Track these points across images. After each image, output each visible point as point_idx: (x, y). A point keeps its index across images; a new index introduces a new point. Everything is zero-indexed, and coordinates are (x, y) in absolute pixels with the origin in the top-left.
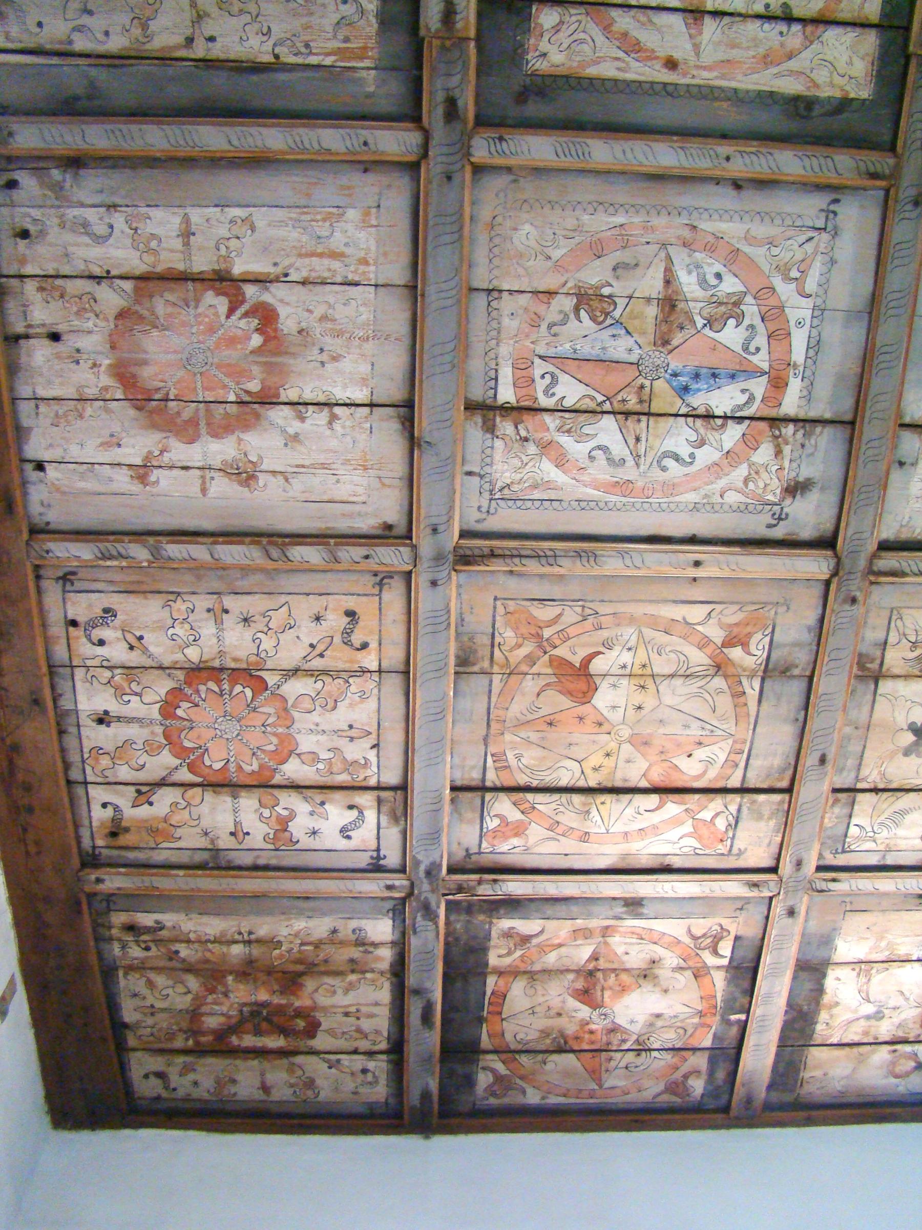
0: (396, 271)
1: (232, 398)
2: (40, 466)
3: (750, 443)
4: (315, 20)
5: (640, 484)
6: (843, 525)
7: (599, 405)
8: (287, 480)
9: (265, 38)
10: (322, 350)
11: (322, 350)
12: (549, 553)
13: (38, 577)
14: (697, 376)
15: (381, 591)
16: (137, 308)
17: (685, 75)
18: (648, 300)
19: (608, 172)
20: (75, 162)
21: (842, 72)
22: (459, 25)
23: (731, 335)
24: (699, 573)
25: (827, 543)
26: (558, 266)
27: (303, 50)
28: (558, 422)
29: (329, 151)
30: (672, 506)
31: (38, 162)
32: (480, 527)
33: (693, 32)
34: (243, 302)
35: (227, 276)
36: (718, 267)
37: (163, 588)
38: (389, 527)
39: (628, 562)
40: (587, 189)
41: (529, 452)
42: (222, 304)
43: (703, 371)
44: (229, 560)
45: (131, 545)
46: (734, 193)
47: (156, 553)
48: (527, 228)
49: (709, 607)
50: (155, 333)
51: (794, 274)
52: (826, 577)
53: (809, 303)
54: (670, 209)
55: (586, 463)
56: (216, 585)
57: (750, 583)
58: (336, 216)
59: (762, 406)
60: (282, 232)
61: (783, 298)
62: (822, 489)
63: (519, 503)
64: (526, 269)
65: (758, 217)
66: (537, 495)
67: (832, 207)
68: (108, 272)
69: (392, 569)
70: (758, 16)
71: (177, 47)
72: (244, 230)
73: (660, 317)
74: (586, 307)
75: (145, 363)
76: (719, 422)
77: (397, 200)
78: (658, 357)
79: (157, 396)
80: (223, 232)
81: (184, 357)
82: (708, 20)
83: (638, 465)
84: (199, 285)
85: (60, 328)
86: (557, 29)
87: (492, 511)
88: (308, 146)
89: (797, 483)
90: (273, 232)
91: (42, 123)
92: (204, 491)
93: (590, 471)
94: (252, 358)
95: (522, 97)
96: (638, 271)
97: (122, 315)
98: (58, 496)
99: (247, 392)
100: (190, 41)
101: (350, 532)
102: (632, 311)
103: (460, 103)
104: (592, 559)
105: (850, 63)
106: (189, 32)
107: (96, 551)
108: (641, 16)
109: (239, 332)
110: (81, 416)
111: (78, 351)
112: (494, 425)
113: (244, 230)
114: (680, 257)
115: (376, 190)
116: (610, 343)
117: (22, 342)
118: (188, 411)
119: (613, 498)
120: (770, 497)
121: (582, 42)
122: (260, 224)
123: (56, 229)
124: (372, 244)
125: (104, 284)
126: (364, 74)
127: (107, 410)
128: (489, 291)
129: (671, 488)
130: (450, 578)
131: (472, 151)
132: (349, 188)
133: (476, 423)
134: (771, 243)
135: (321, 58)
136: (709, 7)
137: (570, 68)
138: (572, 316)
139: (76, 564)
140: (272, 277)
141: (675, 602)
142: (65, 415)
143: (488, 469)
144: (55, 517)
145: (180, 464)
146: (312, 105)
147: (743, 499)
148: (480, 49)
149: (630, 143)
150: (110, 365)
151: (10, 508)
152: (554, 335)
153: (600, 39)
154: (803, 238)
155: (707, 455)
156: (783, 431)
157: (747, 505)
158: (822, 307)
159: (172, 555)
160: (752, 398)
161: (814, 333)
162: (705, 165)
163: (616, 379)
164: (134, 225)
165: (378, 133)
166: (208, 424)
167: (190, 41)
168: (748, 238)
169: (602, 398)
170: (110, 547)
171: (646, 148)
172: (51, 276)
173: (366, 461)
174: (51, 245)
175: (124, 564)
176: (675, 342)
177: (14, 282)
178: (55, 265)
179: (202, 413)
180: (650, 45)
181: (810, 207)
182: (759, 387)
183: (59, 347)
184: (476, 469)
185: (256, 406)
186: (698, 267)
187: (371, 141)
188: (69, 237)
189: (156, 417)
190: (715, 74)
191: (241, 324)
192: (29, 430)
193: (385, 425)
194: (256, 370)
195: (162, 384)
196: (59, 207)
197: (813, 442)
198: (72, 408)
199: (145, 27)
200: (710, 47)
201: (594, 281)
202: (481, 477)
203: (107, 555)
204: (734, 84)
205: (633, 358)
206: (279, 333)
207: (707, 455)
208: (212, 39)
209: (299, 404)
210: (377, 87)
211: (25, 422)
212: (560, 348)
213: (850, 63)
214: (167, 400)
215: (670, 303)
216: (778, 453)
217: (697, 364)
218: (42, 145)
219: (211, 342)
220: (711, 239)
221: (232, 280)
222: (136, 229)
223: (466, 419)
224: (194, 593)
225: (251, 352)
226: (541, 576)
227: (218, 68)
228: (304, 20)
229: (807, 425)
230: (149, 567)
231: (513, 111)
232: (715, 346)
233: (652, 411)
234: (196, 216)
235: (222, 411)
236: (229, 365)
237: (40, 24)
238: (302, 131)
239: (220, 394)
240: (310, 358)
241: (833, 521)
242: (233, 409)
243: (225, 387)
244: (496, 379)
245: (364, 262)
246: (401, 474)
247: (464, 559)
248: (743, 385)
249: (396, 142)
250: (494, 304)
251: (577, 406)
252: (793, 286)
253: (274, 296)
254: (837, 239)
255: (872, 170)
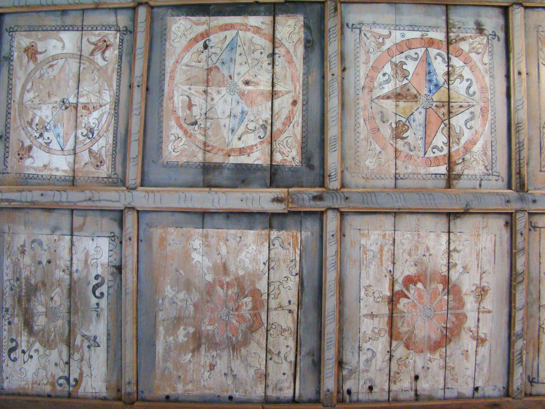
0: (388, 221)
1: (446, 297)
2: (476, 389)
3: (459, 53)
4: (282, 258)
5: (482, 104)
6: (496, 4)
7: (446, 126)
8: (484, 272)
9: (289, 279)
10: (424, 255)
11: (424, 255)
12: (517, 146)
13: (531, 395)
14: (430, 81)
15: (538, 227)
16: (404, 339)
17: (299, 97)
18: (397, 106)
19: (342, 127)
20: (340, 364)
21: (293, 29)
22: (283, 196)
23: (410, 67)
24: (524, 72)
25: (505, 11)
26: (384, 148)
27: (294, 263)
28: (454, 145)
29: (336, 252)
30: (492, 88)
31: (340, 380)
32: (506, 179)
33: (281, 95)
34: (402, 291)
35: (391, 298)
36: (380, 75)
37: (537, 333)
38: (507, 224)
39: (520, 107)
40: (349, 136)
41: (469, 157)
42: (403, 301)
43: (428, 78)
44: (523, 301)
45: (515, 348)
46: (347, 70)
47: (520, 336)
48: (367, 163)
49: (541, 65)
50: (416, 332)
51: (381, 40)
52: (522, 8)
53: (393, 32)
54: (356, 99)
55: (473, 131)
56: (535, 307)
57: (527, 46)
58: (365, 250)
59: (442, 49)
60: (372, 273)
61: (392, 44)
62: (479, 16)
63: (494, 161)
64: (386, 163)
65: (357, 59)
66: (489, 153)
67: (350, 26)
68: (388, 352)
69: (527, 222)
70: (273, 68)
71: (293, 318)
72: (370, 290)
73: (404, 100)
74: (401, 134)
75: (429, 337)
76: (451, 69)
77: (354, 221)
78: (422, 99)
79: (445, 332)
80: (371, 299)
81: (427, 319)
82: (275, 89)
83: (473, 106)
84: (395, 311)
85: (413, 375)
86: (282, 153)
87: (498, 174)
88: (334, 261)
89: (477, 29)
90: (371, 277)
91: (324, 377)
92: (489, 312)
93: (477, 129)
94: (428, 287)
95: (311, 167)
96: (385, 112)
97: (407, 347)
98: (490, 382)
99: (443, 290)
100: (290, 311)
101: (509, 242)
102: (402, 113)
103: (315, 194)
104: (520, 125)
105: (289, 26)
106: (287, 312)
107: (518, 365)
108: (275, 118)
109: (416, 293)
110: (453, 368)
111: (423, 367)
112: (457, 175)
113: (370, 290)
114: (378, 93)
115: (352, 231)
116: (417, 122)
117: (418, 393)
118: (452, 318)
119: (490, 117)
120: (485, 41)
121: (287, 142)
122: (368, 283)
123: (369, 374)
124: (377, 232)
125: (393, 354)
126: (303, 236)
127: (451, 355)
128: (396, 179)
129: (483, 89)
130: (531, 194)
131: (335, 188)
132: (352, 243)
133: (457, 183)
134: (368, 52)
135: (297, 255)
136: (271, 88)
137: (298, 146)
138: (406, 140)
139: (524, 376)
140: (391, 278)
141: (539, 82)
142: (452, 375)
143: (478, 177)
144: (501, 384)
145: (477, 323)
146: (317, 260)
147: (487, 54)
148: (292, 187)
149: (328, 118)
150: (430, 353)
151: (496, 405)
152: (415, 148)
153: (285, 135)
154: (365, 38)
155: (467, 73)
156: (453, 38)
157: (490, 52)
158: (394, 26)
159: (521, 329)
160: (439, 54)
161: (407, 28)
162: (337, 85)
163: (433, 119)
164: (368, 339)
165: (328, 230)
166: (458, 309)
167: (290, 311)
168: (366, 63)
169: (443, 125)
170: (516, 359)
171: (331, 112)
172: (389, 378)
173: (475, 235)
174: (375, 377)
175: (524, 352)
176: (415, 92)
177: (391, 394)
178: (385, 376)
179: (453, 311)
180: (287, 113)
181: (351, 36)
182: (433, 52)
183: (421, 376)
184: (478, 182)
185: (450, 286)
186: (381, 84)
187: (332, 233)
188: (372, 368)
189: (455, 333)
190: (297, 84)
191: (412, 292)
192: (458, 393)
193: (458, 226)
194: (433, 286)
195: (439, 330)
196: (359, 372)
197: (457, 23)
198: (449, 372)
199: (285, 330)
200: (286, 87)
201: (390, 131)
202: (482, 180)
203: (520, 360)
204: (301, 75)
205: (423, 111)
206: (417, 275)
207: (467, 73)
208: (290, 302)
209: (449, 266)
210: (308, 231)
211: (455, 394)
212: (421, 145)
213: (289, 26)
214: (446, 328)
215: (398, 96)
216: (463, 39)
217: (424, 81)
218: (333, 378)
219: (420, 306)
220: (368, 79)
221: (393, 296)
222: (370, 338)
223: (455, 188)
224: (539, 319)
225: (425, 288)
226: (529, 149)
227: (301, 301)
228: (282, 262)
229: (449, 27)
230: (526, 340)
231: (317, 170)
232: (416, 73)
233: (447, 100)
234: (364, 311)
235: (452, 302)
236: (431, 298)
237: (284, 374)
238: (328, 263)
239: (444, 303)
240: (428, 261)
241: (494, 9)
242: (451, 297)
243: (441, 300)
244: (435, 174)
245: (384, 236)
246: (481, 219)
247: (522, 187)
248: (433, 59)
249: (332, 222)
250: (402, 176)
251: (447, 136)
252: (386, 40)
253: (400, 277)
254: (364, 23)
255: (333, 11)
